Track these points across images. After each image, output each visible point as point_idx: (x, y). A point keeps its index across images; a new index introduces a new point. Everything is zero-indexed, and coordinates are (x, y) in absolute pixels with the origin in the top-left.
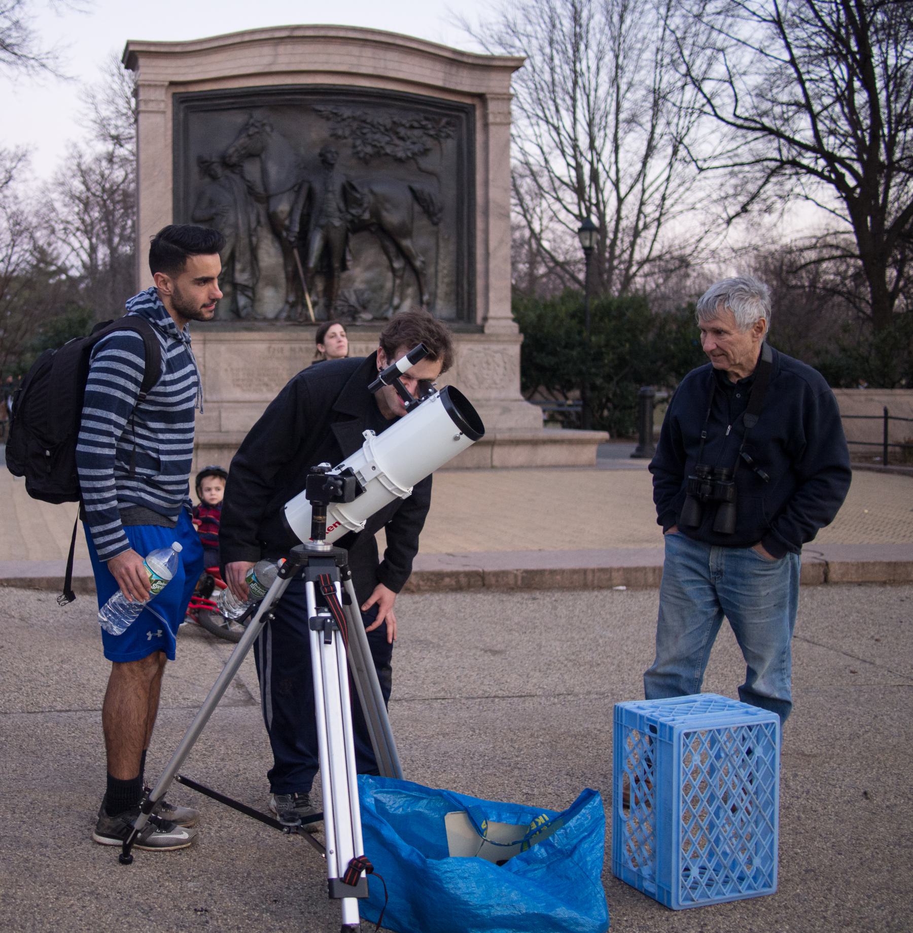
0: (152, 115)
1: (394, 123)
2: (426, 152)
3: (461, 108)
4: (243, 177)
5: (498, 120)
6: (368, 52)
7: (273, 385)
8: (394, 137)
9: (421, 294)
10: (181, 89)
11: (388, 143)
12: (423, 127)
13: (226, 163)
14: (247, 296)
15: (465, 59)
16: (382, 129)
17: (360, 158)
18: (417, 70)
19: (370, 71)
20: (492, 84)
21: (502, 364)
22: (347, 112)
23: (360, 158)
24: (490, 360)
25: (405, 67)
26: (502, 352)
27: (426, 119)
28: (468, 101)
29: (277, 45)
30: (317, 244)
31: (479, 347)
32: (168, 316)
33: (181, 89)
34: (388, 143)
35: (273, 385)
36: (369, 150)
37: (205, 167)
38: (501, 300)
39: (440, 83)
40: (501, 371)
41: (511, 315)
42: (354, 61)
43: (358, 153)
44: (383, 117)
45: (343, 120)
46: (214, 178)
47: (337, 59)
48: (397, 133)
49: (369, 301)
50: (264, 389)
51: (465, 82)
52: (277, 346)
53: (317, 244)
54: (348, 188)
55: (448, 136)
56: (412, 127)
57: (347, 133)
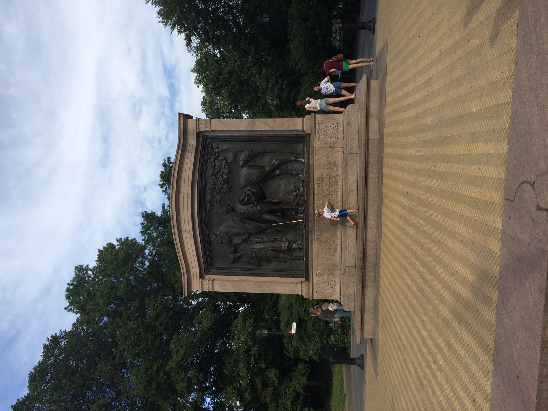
0: (214, 286)
1: (213, 175)
2: (225, 159)
3: (204, 142)
4: (240, 244)
5: (208, 126)
6: (182, 189)
7: (334, 240)
8: (219, 174)
9: (292, 161)
10: (203, 271)
11: (222, 177)
12: (214, 161)
13: (235, 251)
14: (293, 243)
15: (181, 144)
16: (216, 180)
17: (230, 191)
18: (188, 166)
19: (190, 188)
20: (192, 129)
21: (325, 124)
22: (209, 197)
23: (230, 191)
24: (324, 130)
25: (187, 172)
26: (320, 124)
27: (210, 159)
28: (201, 138)
29: (181, 231)
30: (268, 217)
31: (317, 136)
32: (303, 158)
33: (203, 271)
34: (222, 177)
35: (334, 240)
36: (225, 186)
37: (235, 261)
38: (294, 124)
39: (193, 155)
40: (329, 125)
41: (301, 119)
42: (186, 196)
43: (227, 191)
44: (210, 181)
45: (213, 198)
46: (240, 257)
47: (185, 203)
48: (217, 173)
49: (295, 186)
50: (336, 243)
51: (192, 142)
52: (315, 238)
53: (268, 217)
54: (244, 203)
55: (218, 148)
56: (214, 166)
57: (219, 196)
